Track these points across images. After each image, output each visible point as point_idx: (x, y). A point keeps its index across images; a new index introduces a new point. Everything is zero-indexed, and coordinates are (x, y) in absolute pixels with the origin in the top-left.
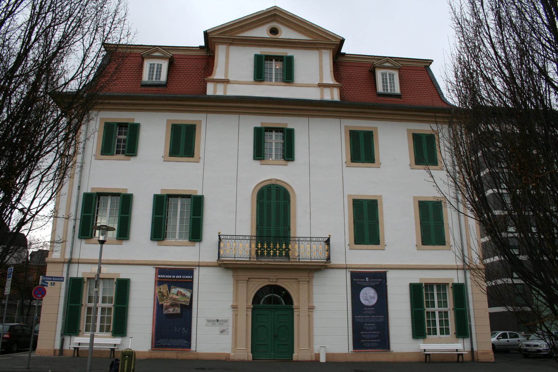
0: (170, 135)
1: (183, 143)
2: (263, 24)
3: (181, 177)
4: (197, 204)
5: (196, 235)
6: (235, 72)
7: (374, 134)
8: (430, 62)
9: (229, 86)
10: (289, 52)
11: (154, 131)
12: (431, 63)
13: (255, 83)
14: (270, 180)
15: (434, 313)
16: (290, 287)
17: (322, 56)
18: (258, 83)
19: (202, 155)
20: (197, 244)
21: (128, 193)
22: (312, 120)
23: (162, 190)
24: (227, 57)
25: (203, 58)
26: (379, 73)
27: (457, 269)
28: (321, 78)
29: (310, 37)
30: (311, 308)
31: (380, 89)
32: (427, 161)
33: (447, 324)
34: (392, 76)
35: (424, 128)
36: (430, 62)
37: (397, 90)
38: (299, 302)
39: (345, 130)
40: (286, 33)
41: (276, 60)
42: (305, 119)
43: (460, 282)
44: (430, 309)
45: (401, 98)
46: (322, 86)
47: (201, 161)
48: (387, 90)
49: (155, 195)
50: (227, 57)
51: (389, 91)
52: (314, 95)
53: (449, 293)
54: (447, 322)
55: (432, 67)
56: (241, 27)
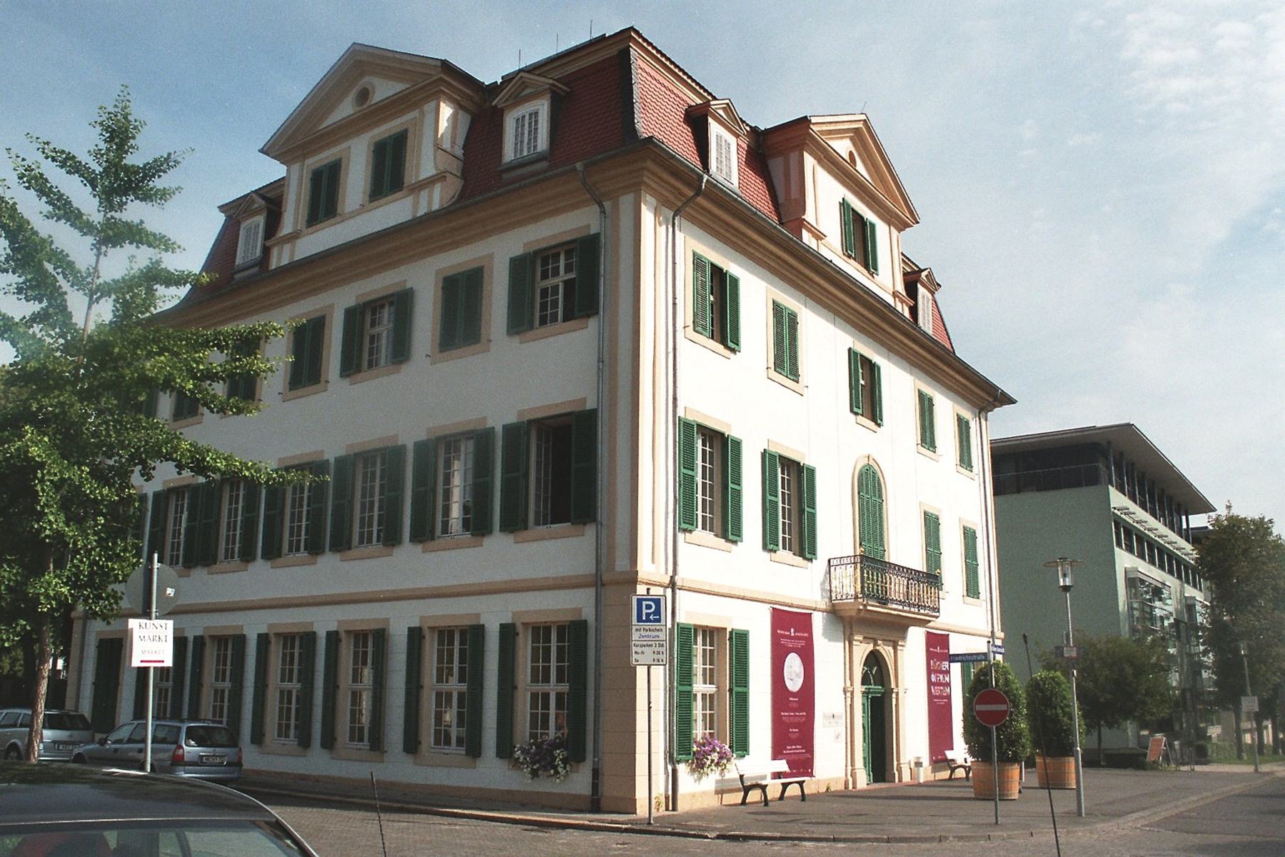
15: (546, 696)
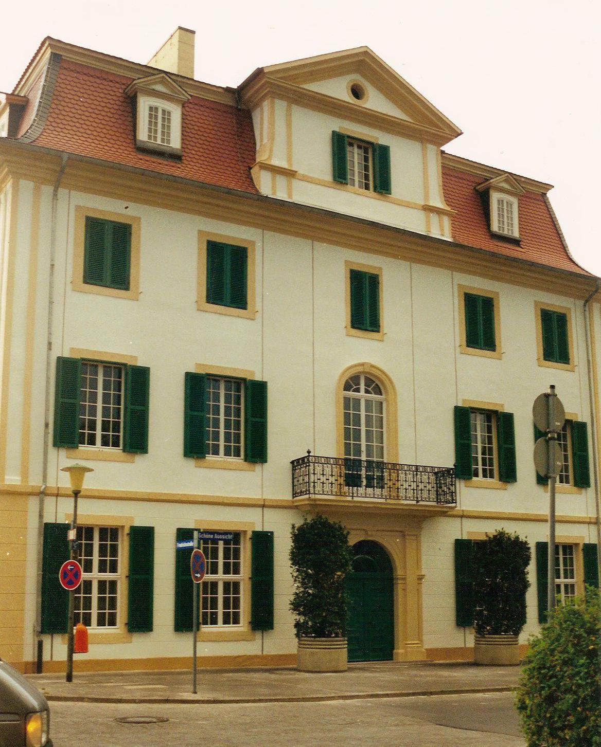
0: (83, 238)
1: (227, 279)
2: (341, 74)
3: (226, 344)
4: (254, 395)
5: (256, 452)
6: (295, 153)
7: (495, 303)
8: (549, 187)
9: (296, 183)
10: (382, 138)
11: (169, 251)
12: (549, 189)
13: (333, 185)
14: (363, 364)
15: (214, 585)
16: (392, 544)
17: (291, 115)
18: (338, 187)
19: (258, 307)
20: (258, 467)
21: (139, 364)
22: (416, 267)
23: (198, 365)
24: (289, 125)
25: (231, 116)
26: (144, 104)
27: (589, 523)
28: (426, 196)
29: (411, 116)
30: (420, 578)
31: (143, 135)
32: (229, 300)
33: (113, 605)
34: (510, 205)
35: (480, 285)
36: (549, 187)
37: (175, 143)
38: (405, 568)
39: (459, 291)
40: (375, 102)
41: (359, 147)
42: (405, 265)
43: (59, 522)
44: (209, 577)
45: (519, 245)
46: (428, 209)
47: (258, 316)
48: (155, 138)
49: (148, 369)
50: (289, 125)
51: (159, 142)
52: (415, 223)
53: (577, 560)
54: (113, 601)
55: (550, 194)
56: (312, 73)
